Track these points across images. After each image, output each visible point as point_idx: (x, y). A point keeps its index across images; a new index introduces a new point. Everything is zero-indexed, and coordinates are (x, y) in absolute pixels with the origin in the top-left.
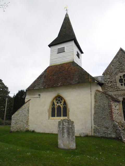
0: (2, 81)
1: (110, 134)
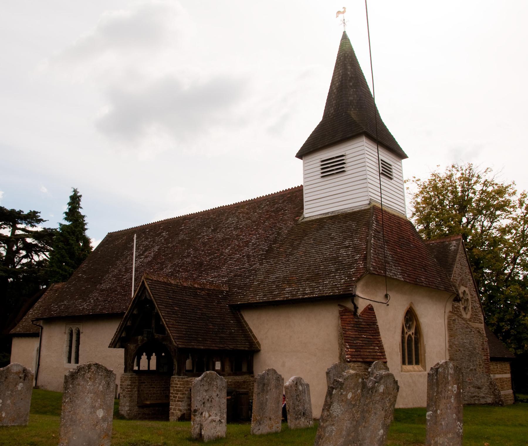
0: (84, 217)
1: (483, 397)
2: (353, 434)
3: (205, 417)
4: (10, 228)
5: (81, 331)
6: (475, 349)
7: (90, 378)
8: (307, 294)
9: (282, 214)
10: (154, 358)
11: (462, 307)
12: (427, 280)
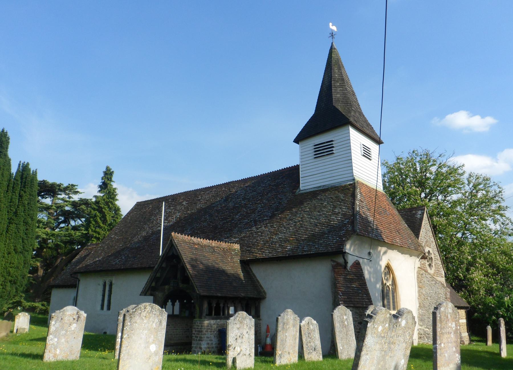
4: (51, 198)
5: (113, 282)
7: (145, 317)
8: (305, 251)
9: (282, 187)
10: (177, 304)
11: (427, 263)
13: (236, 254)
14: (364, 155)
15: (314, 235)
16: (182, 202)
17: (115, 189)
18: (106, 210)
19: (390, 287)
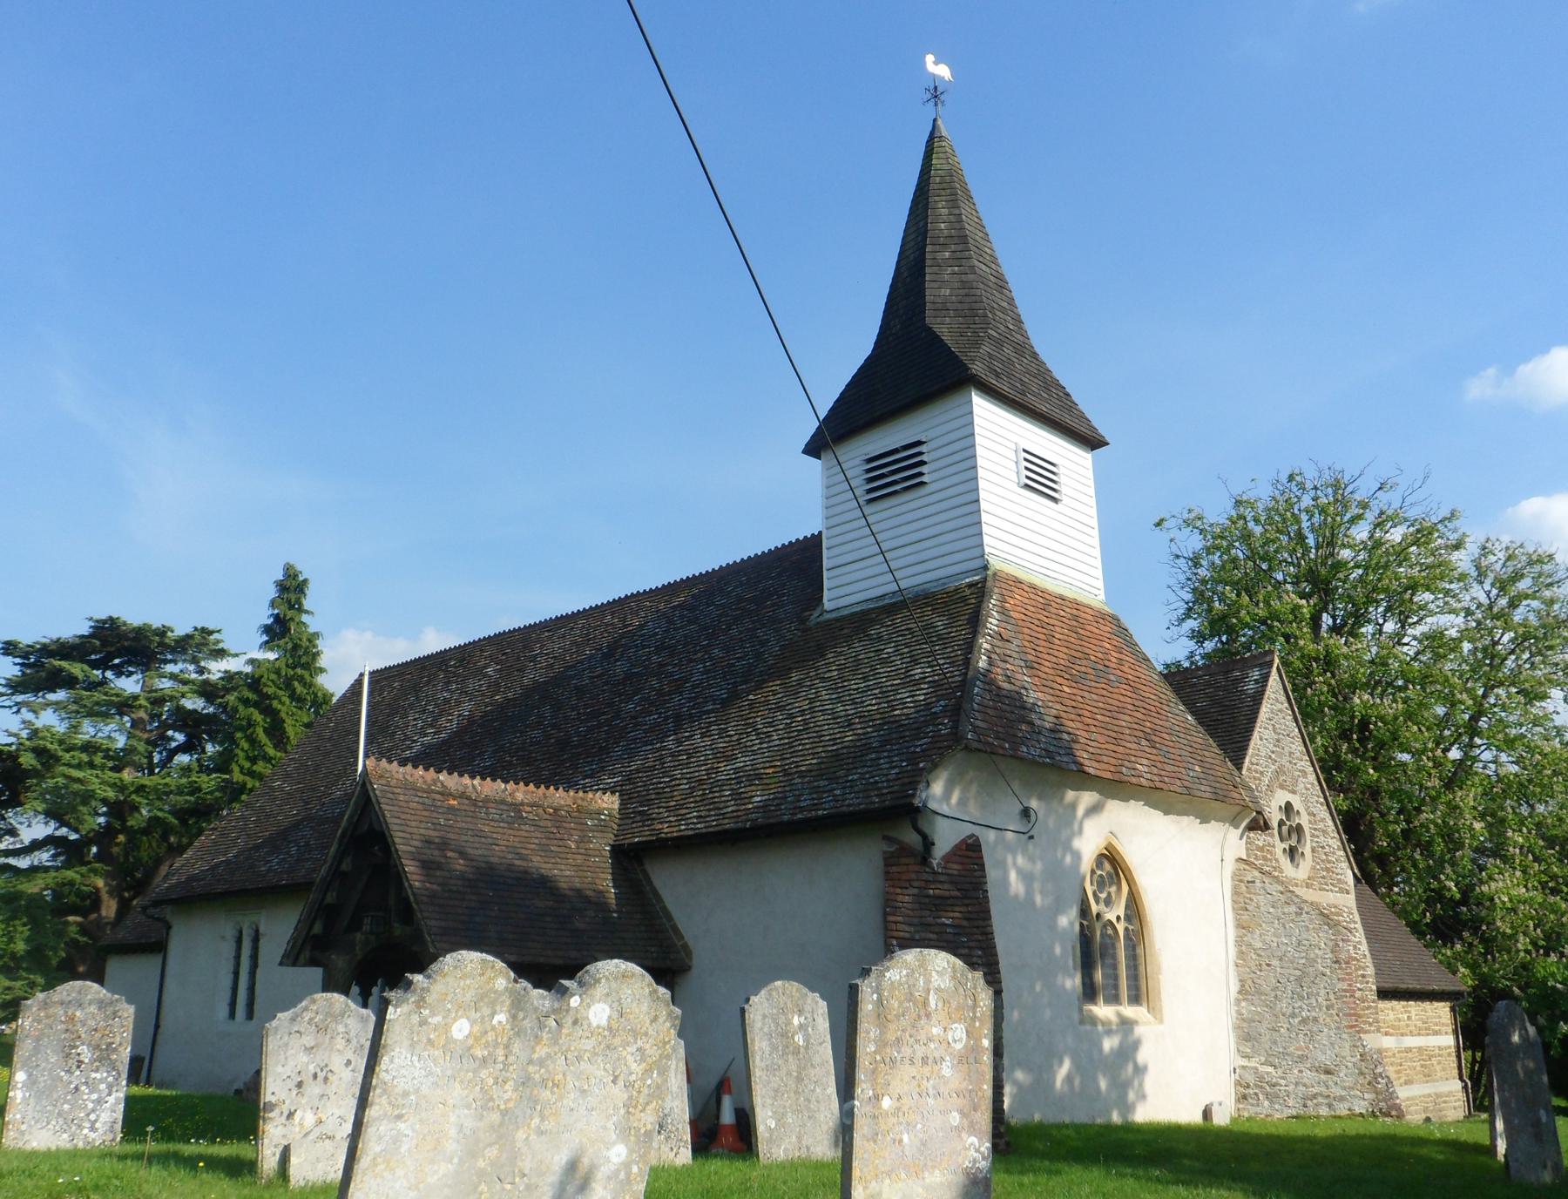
2: (492, 1152)
3: (301, 1125)
6: (1312, 962)
8: (802, 809)
12: (1155, 771)
13: (602, 828)
14: (1027, 486)
15: (836, 756)
16: (486, 667)
17: (316, 635)
18: (284, 706)
19: (1120, 928)
